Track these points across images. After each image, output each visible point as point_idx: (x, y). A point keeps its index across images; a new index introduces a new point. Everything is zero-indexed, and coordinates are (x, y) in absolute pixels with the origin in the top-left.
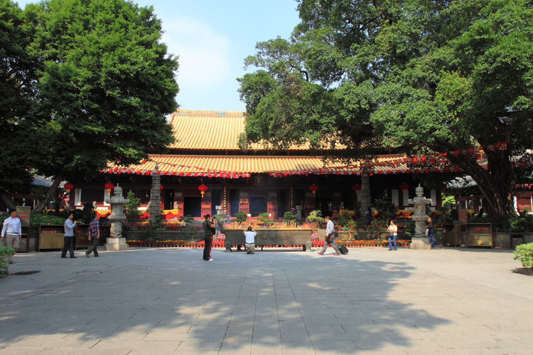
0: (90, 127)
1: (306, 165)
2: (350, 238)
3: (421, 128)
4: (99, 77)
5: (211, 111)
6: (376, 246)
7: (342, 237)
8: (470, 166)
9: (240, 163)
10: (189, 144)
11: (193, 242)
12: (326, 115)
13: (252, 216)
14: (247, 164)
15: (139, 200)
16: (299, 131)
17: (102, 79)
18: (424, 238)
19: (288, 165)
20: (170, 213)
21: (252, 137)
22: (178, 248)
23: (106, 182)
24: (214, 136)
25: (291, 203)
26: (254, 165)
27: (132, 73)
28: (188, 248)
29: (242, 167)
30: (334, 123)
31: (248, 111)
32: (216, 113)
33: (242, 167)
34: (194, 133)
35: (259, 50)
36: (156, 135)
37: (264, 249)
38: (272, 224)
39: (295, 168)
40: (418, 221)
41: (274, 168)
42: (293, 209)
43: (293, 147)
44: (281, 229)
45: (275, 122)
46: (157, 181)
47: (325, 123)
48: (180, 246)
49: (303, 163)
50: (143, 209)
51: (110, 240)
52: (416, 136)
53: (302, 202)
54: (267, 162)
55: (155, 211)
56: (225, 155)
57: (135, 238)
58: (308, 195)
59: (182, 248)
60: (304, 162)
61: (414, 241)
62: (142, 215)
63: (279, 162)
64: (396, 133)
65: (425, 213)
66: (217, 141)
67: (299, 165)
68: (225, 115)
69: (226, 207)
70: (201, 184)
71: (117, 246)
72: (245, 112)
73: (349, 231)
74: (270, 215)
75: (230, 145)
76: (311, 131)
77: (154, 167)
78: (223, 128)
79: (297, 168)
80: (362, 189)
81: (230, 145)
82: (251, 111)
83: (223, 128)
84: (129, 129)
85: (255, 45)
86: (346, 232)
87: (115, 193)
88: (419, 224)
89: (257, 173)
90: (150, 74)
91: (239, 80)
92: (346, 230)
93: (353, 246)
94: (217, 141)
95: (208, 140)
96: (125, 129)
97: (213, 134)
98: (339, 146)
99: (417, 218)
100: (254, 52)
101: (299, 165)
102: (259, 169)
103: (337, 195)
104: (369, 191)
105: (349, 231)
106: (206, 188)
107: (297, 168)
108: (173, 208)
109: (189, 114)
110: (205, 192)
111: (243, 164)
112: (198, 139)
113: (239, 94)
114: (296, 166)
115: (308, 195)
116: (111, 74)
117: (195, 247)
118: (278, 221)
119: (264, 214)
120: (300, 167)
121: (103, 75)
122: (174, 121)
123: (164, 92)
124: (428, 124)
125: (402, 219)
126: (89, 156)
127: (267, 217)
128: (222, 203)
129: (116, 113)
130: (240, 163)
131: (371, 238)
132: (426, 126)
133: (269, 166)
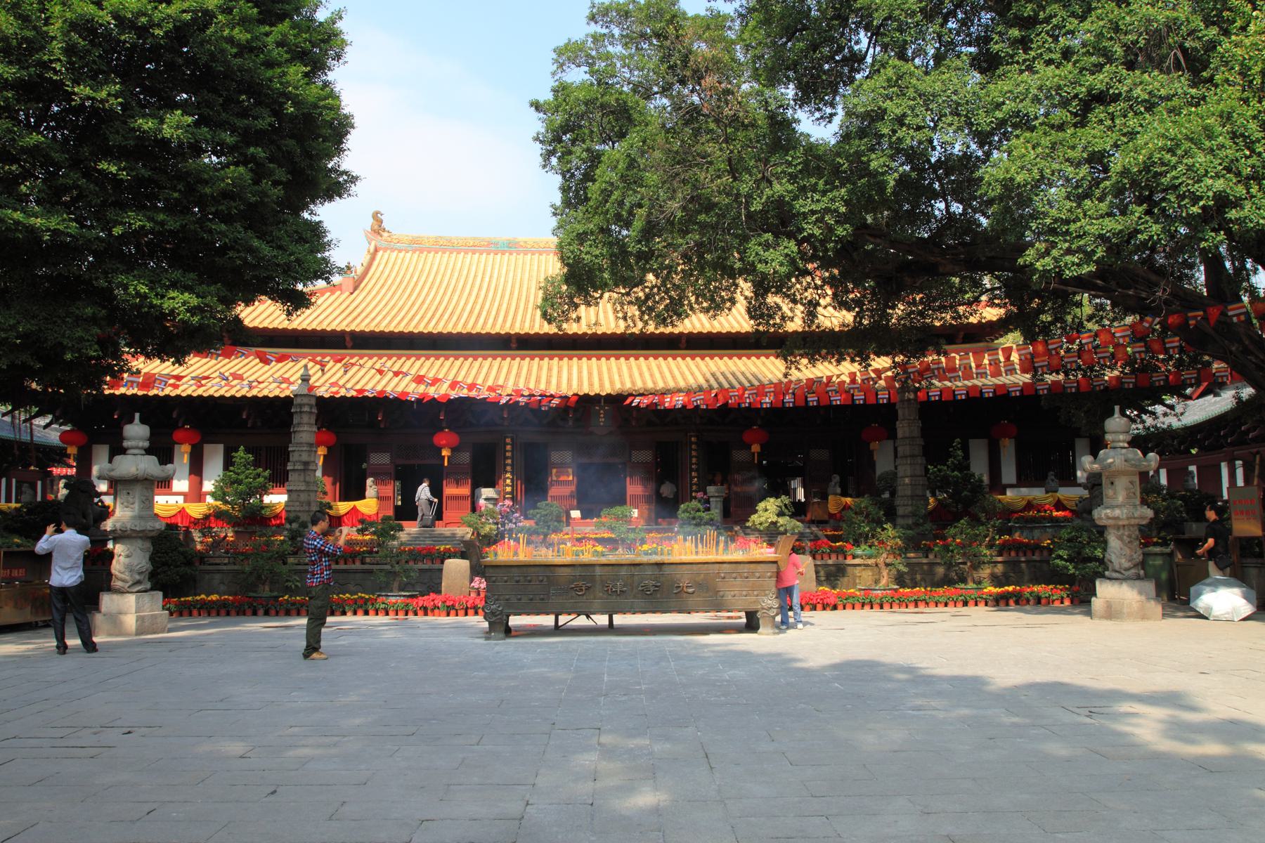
0: (18, 215)
1: (733, 374)
2: (884, 581)
3: (1181, 197)
4: (42, 41)
5: (475, 239)
6: (965, 604)
7: (855, 576)
8: (1252, 353)
9: (550, 369)
10: (411, 320)
11: (395, 599)
12: (814, 189)
13: (584, 517)
14: (570, 374)
15: (267, 473)
16: (714, 270)
17: (57, 46)
18: (1138, 583)
19: (682, 374)
20: (354, 508)
21: (581, 280)
22: (349, 618)
23: (175, 426)
24: (480, 300)
25: (692, 478)
26: (590, 374)
27: (159, 26)
28: (382, 619)
29: (554, 381)
30: (843, 209)
31: (567, 203)
32: (489, 244)
33: (554, 381)
34: (427, 295)
35: (597, 29)
36: (266, 250)
37: (619, 620)
38: (643, 542)
39: (702, 381)
40: (1118, 528)
41: (644, 382)
42: (700, 495)
43: (697, 323)
44: (675, 558)
45: (650, 214)
46: (305, 419)
47: (813, 212)
48: (355, 613)
49: (723, 368)
50: (276, 499)
51: (108, 601)
52: (1156, 228)
53: (719, 478)
54: (625, 368)
55: (302, 504)
56: (510, 349)
57: (223, 588)
58: (739, 456)
59: (360, 619)
60: (726, 365)
61: (1106, 591)
62: (277, 516)
63: (659, 367)
64: (1073, 227)
65: (1138, 502)
66: (489, 313)
67: (713, 375)
68: (512, 247)
69: (512, 493)
70: (442, 430)
71: (130, 621)
72: (558, 202)
73: (881, 560)
74: (635, 513)
75: (523, 321)
76: (769, 236)
77: (298, 375)
78: (506, 282)
79: (707, 381)
80: (900, 434)
81: (523, 321)
82: (574, 196)
83: (506, 282)
84: (162, 223)
85: (587, 12)
86: (870, 562)
87: (126, 444)
88: (1120, 538)
89: (598, 395)
90: (230, 40)
91: (537, 106)
92: (870, 557)
93: (895, 608)
94: (489, 313)
95: (463, 310)
96: (148, 225)
97: (477, 297)
98: (833, 318)
99: (1117, 518)
100: (581, 30)
101: (713, 375)
102: (602, 385)
103: (820, 455)
104: (920, 442)
105: (881, 560)
106: (454, 438)
107: (707, 381)
108: (362, 497)
109: (417, 246)
110: (453, 450)
111: (559, 372)
112: (437, 309)
113: (538, 148)
114: (704, 376)
115: (739, 456)
116: (85, 27)
117: (401, 616)
118: (658, 531)
119: (618, 510)
120: (716, 379)
121: (55, 29)
122: (375, 263)
123: (282, 105)
124: (1210, 182)
125: (1033, 520)
126: (33, 317)
127: (626, 519)
128: (501, 482)
129: (114, 169)
130: (550, 369)
131: (947, 581)
132: (1198, 189)
133: (631, 376)
